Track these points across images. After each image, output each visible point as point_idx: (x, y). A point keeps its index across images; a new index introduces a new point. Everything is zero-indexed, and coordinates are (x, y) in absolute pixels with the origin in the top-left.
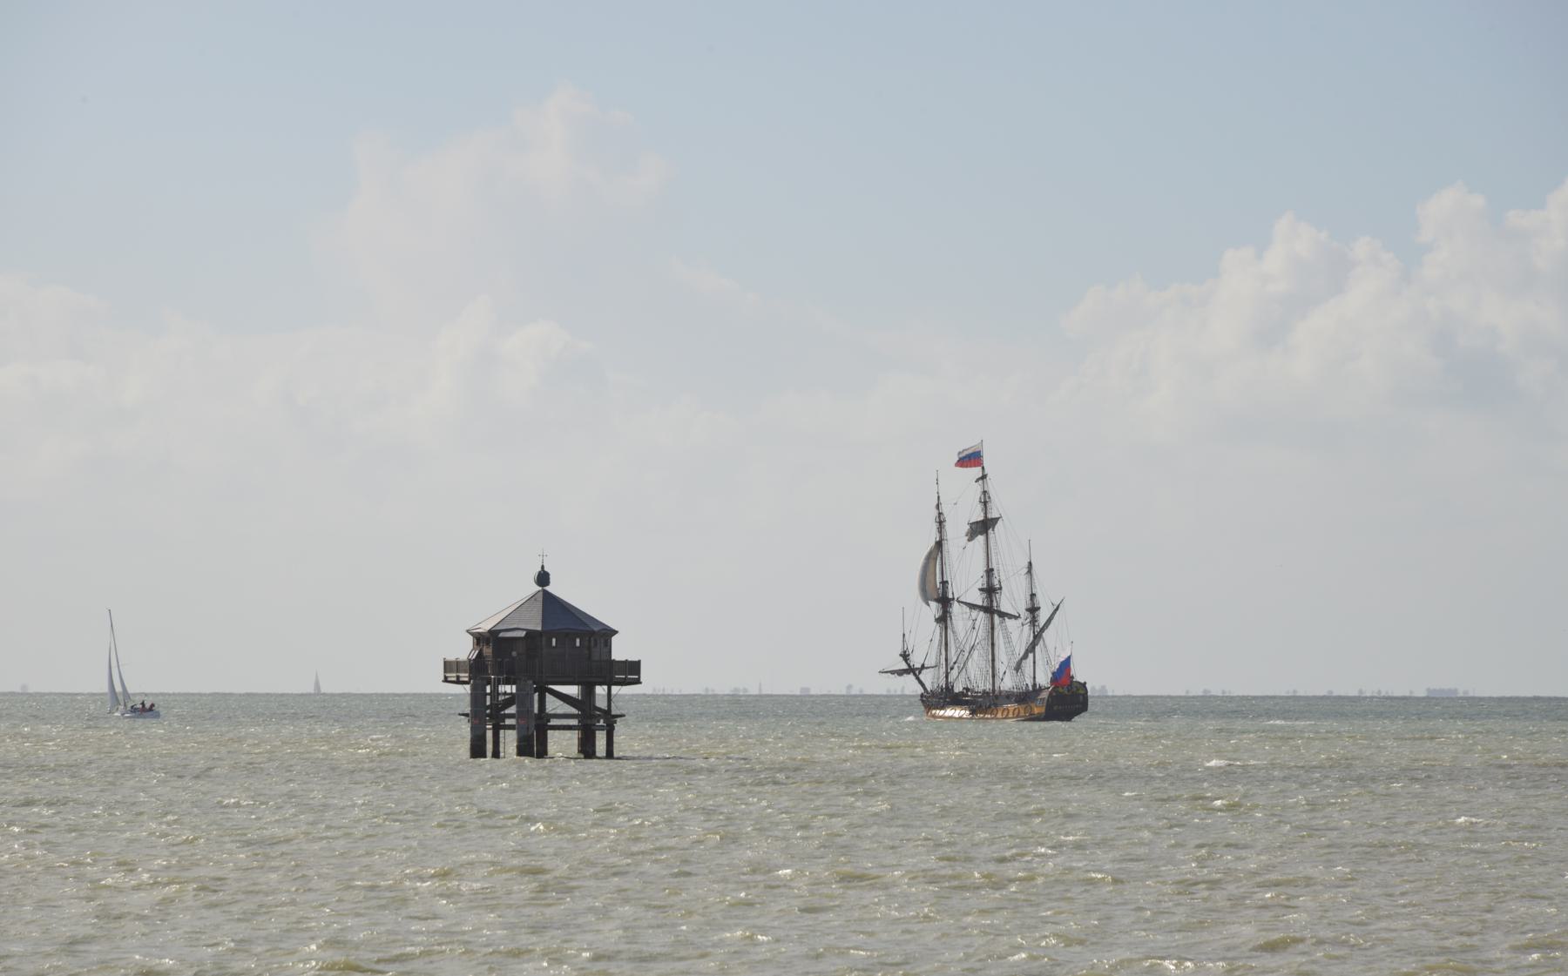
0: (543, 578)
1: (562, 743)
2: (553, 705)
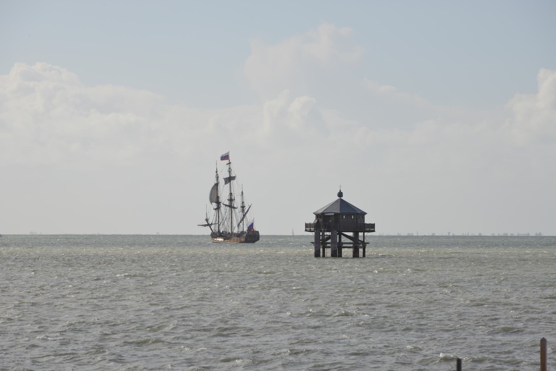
0: (340, 194)
1: (347, 252)
2: (344, 239)
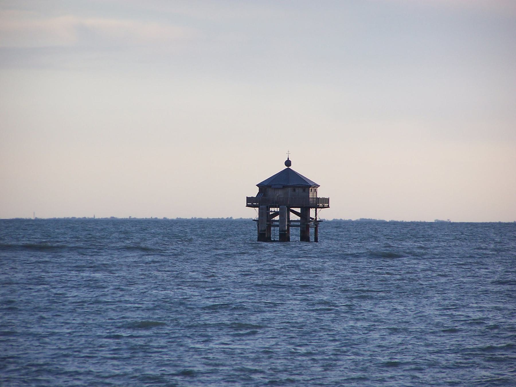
0: (288, 163)
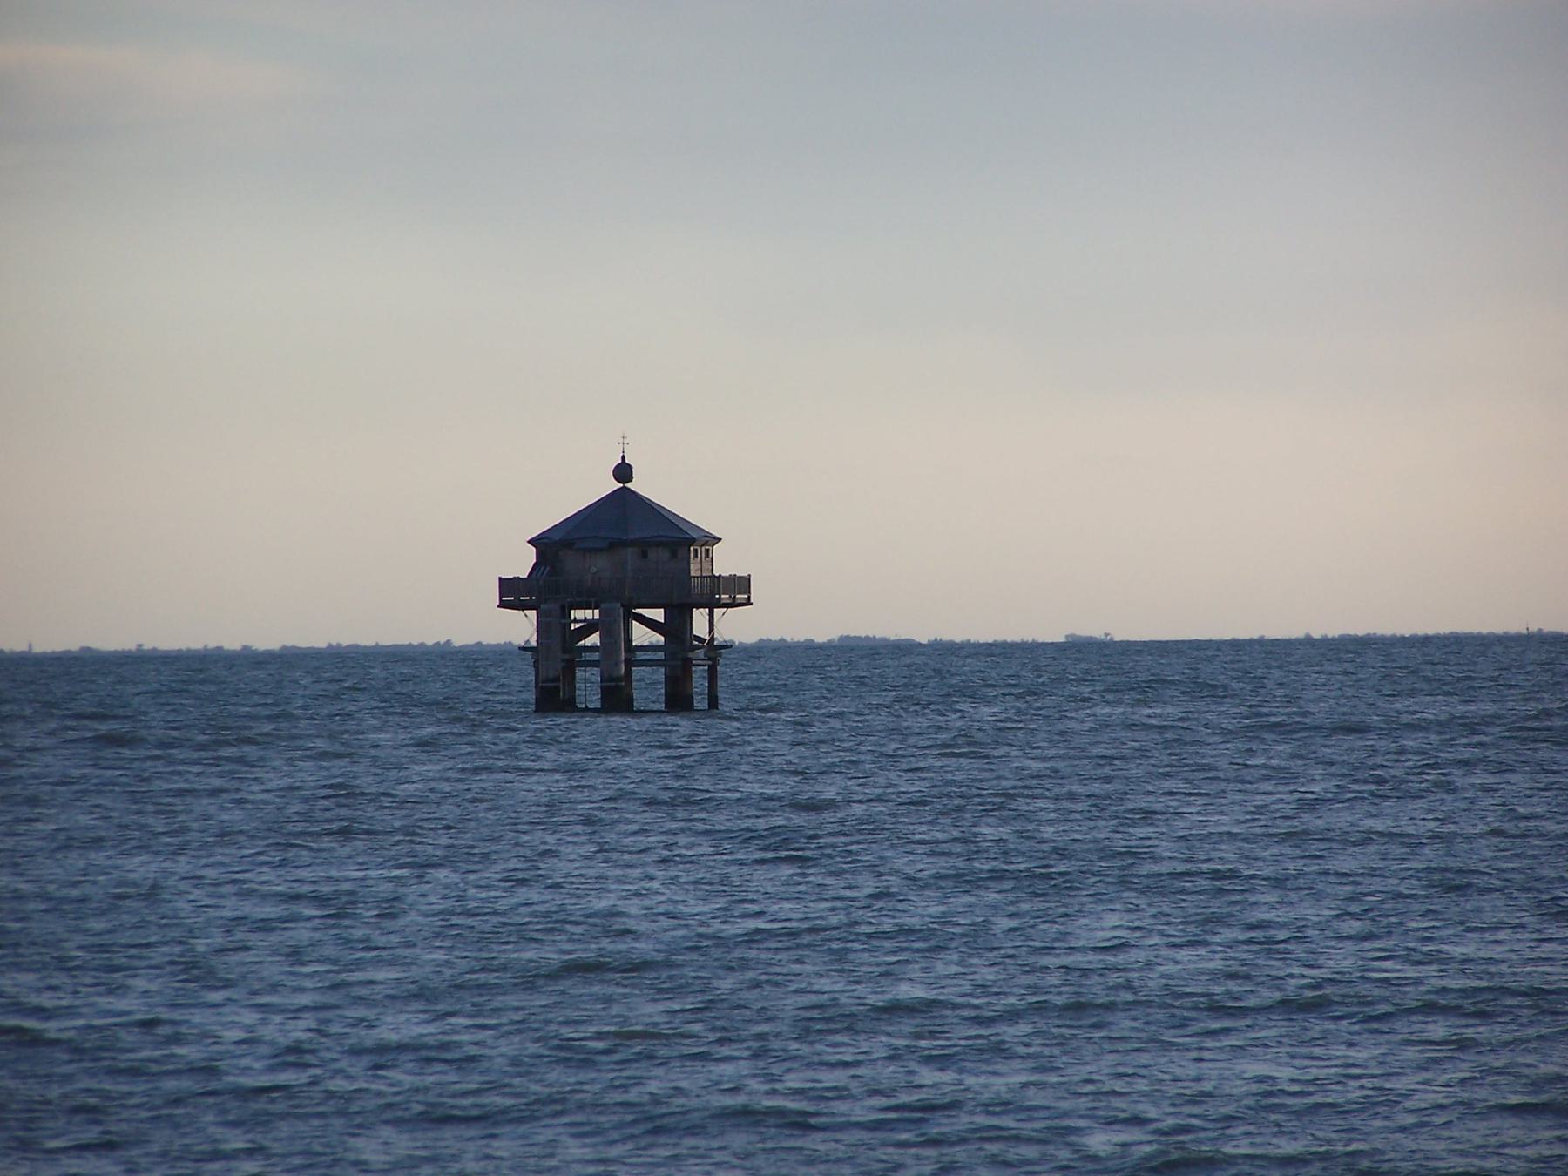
0: (623, 472)
